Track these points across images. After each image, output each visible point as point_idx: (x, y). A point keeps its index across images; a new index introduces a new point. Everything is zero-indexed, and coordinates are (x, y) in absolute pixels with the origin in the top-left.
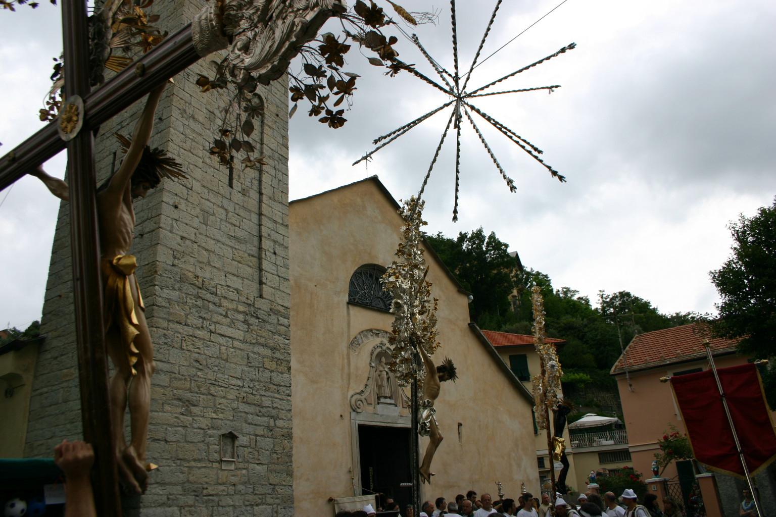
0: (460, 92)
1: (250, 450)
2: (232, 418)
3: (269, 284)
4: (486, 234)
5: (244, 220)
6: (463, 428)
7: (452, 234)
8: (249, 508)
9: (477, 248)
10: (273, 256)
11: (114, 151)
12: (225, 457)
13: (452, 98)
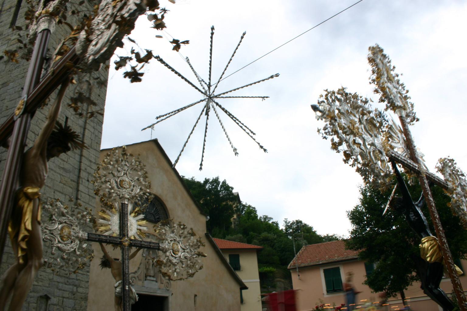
0: (210, 94)
1: (58, 307)
2: (47, 285)
3: (82, 199)
4: (221, 180)
5: (71, 158)
6: (197, 298)
7: (200, 178)
9: (215, 188)
10: (87, 183)
13: (205, 97)
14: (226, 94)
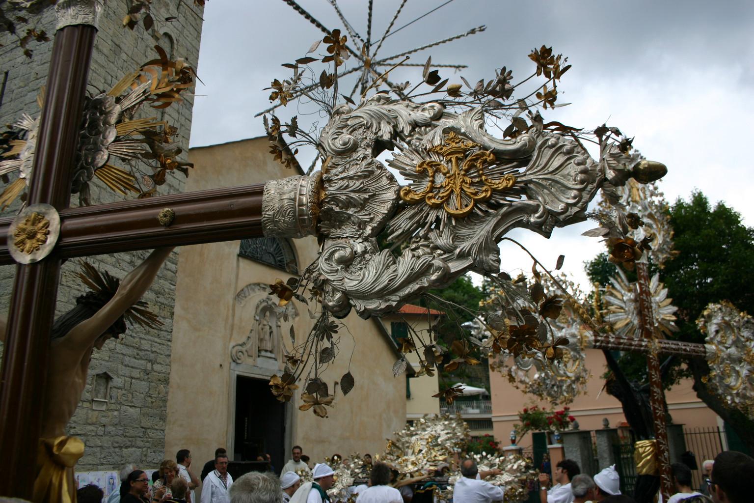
1: (124, 392)
2: (107, 358)
8: (117, 450)
11: (6, 71)
12: (97, 397)
14: (395, 59)
